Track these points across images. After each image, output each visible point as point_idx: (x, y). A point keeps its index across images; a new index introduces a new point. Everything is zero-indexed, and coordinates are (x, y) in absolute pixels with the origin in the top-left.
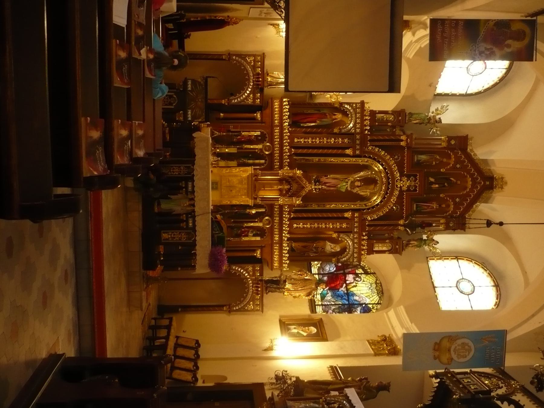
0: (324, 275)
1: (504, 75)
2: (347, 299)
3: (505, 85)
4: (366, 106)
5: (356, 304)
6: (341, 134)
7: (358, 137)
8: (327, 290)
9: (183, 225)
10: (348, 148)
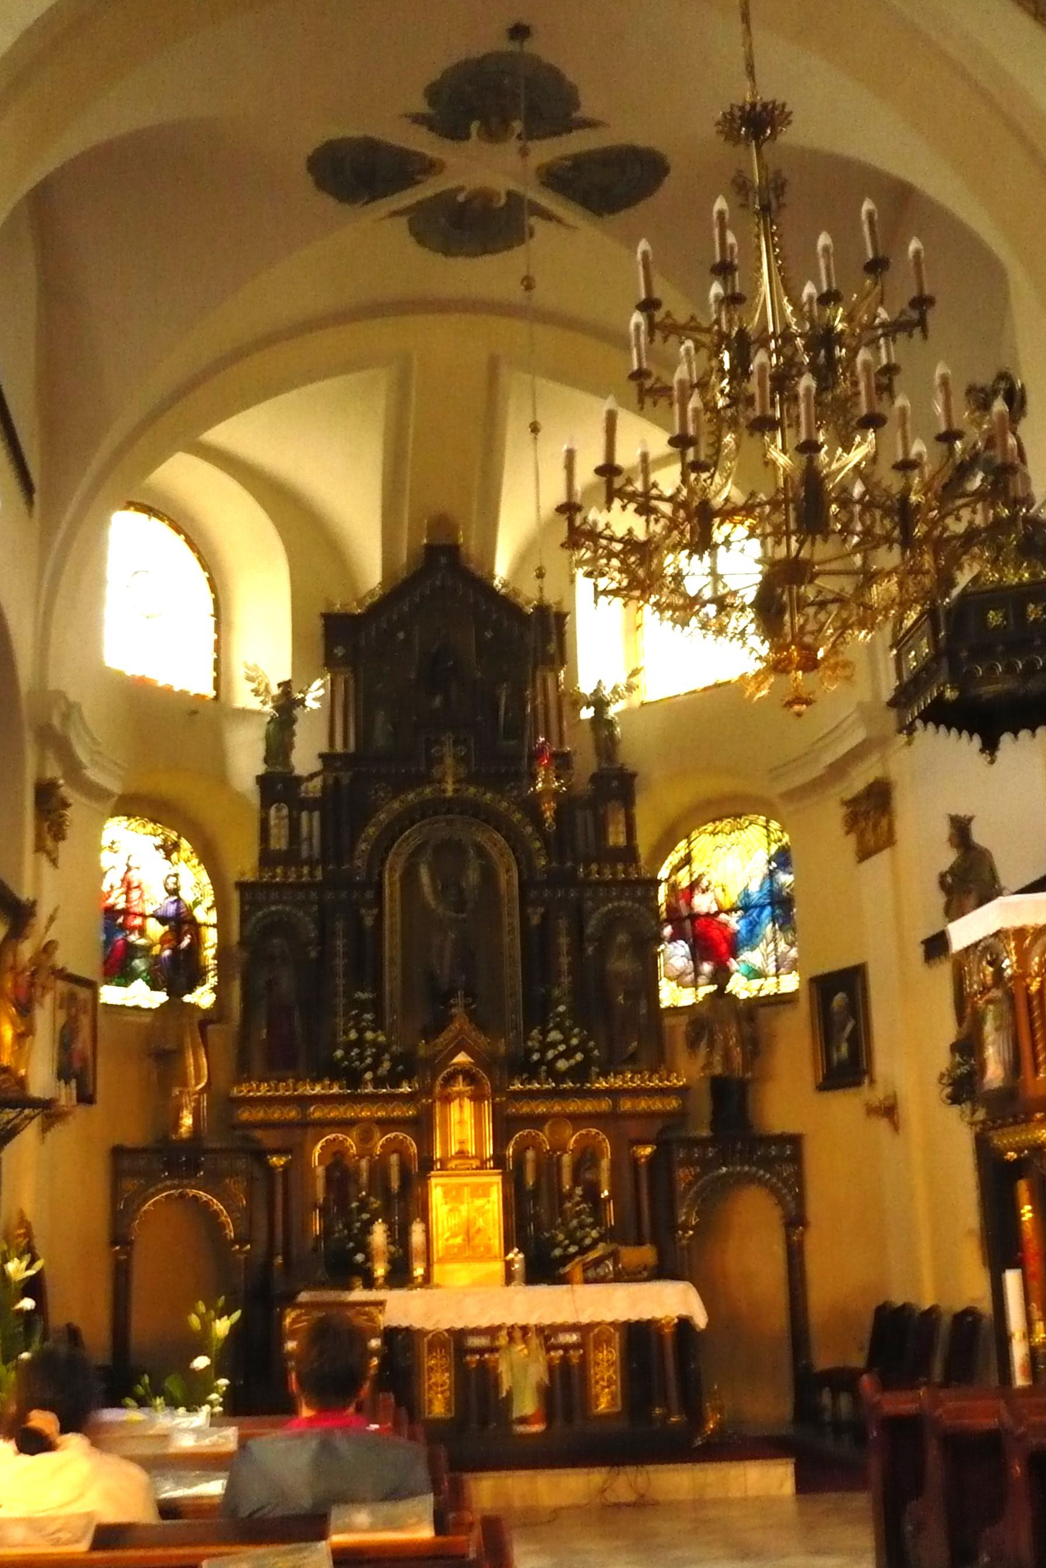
0: (697, 972)
1: (167, 522)
2: (758, 909)
3: (192, 520)
4: (249, 877)
5: (771, 885)
6: (325, 935)
7: (329, 896)
8: (738, 963)
9: (575, 1356)
10: (360, 919)
